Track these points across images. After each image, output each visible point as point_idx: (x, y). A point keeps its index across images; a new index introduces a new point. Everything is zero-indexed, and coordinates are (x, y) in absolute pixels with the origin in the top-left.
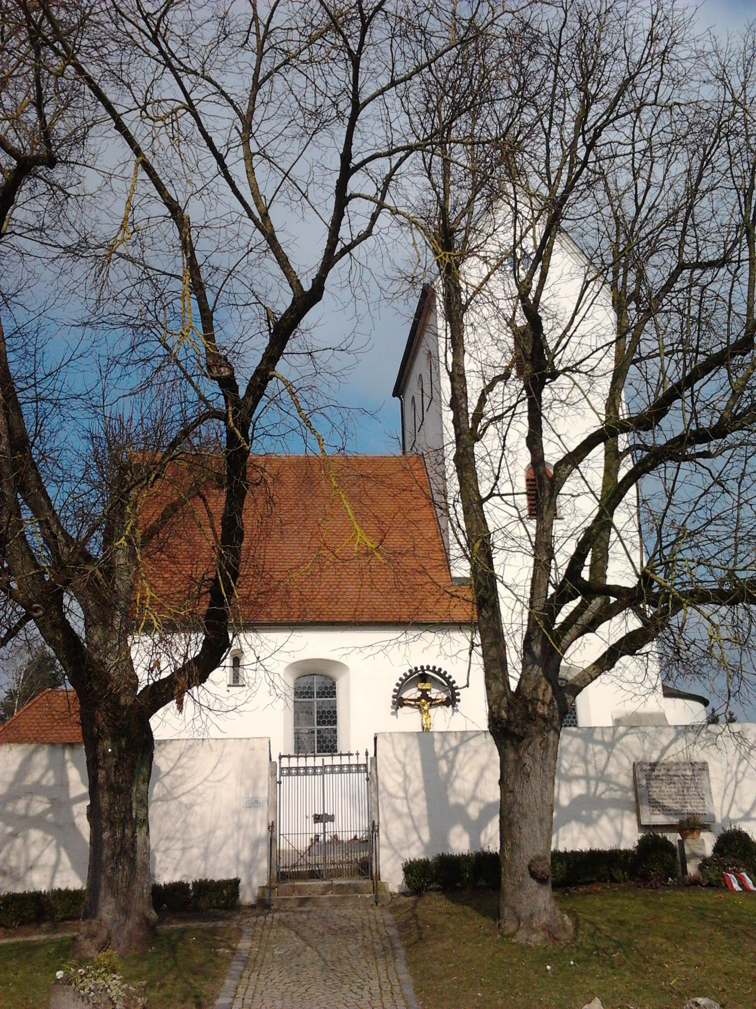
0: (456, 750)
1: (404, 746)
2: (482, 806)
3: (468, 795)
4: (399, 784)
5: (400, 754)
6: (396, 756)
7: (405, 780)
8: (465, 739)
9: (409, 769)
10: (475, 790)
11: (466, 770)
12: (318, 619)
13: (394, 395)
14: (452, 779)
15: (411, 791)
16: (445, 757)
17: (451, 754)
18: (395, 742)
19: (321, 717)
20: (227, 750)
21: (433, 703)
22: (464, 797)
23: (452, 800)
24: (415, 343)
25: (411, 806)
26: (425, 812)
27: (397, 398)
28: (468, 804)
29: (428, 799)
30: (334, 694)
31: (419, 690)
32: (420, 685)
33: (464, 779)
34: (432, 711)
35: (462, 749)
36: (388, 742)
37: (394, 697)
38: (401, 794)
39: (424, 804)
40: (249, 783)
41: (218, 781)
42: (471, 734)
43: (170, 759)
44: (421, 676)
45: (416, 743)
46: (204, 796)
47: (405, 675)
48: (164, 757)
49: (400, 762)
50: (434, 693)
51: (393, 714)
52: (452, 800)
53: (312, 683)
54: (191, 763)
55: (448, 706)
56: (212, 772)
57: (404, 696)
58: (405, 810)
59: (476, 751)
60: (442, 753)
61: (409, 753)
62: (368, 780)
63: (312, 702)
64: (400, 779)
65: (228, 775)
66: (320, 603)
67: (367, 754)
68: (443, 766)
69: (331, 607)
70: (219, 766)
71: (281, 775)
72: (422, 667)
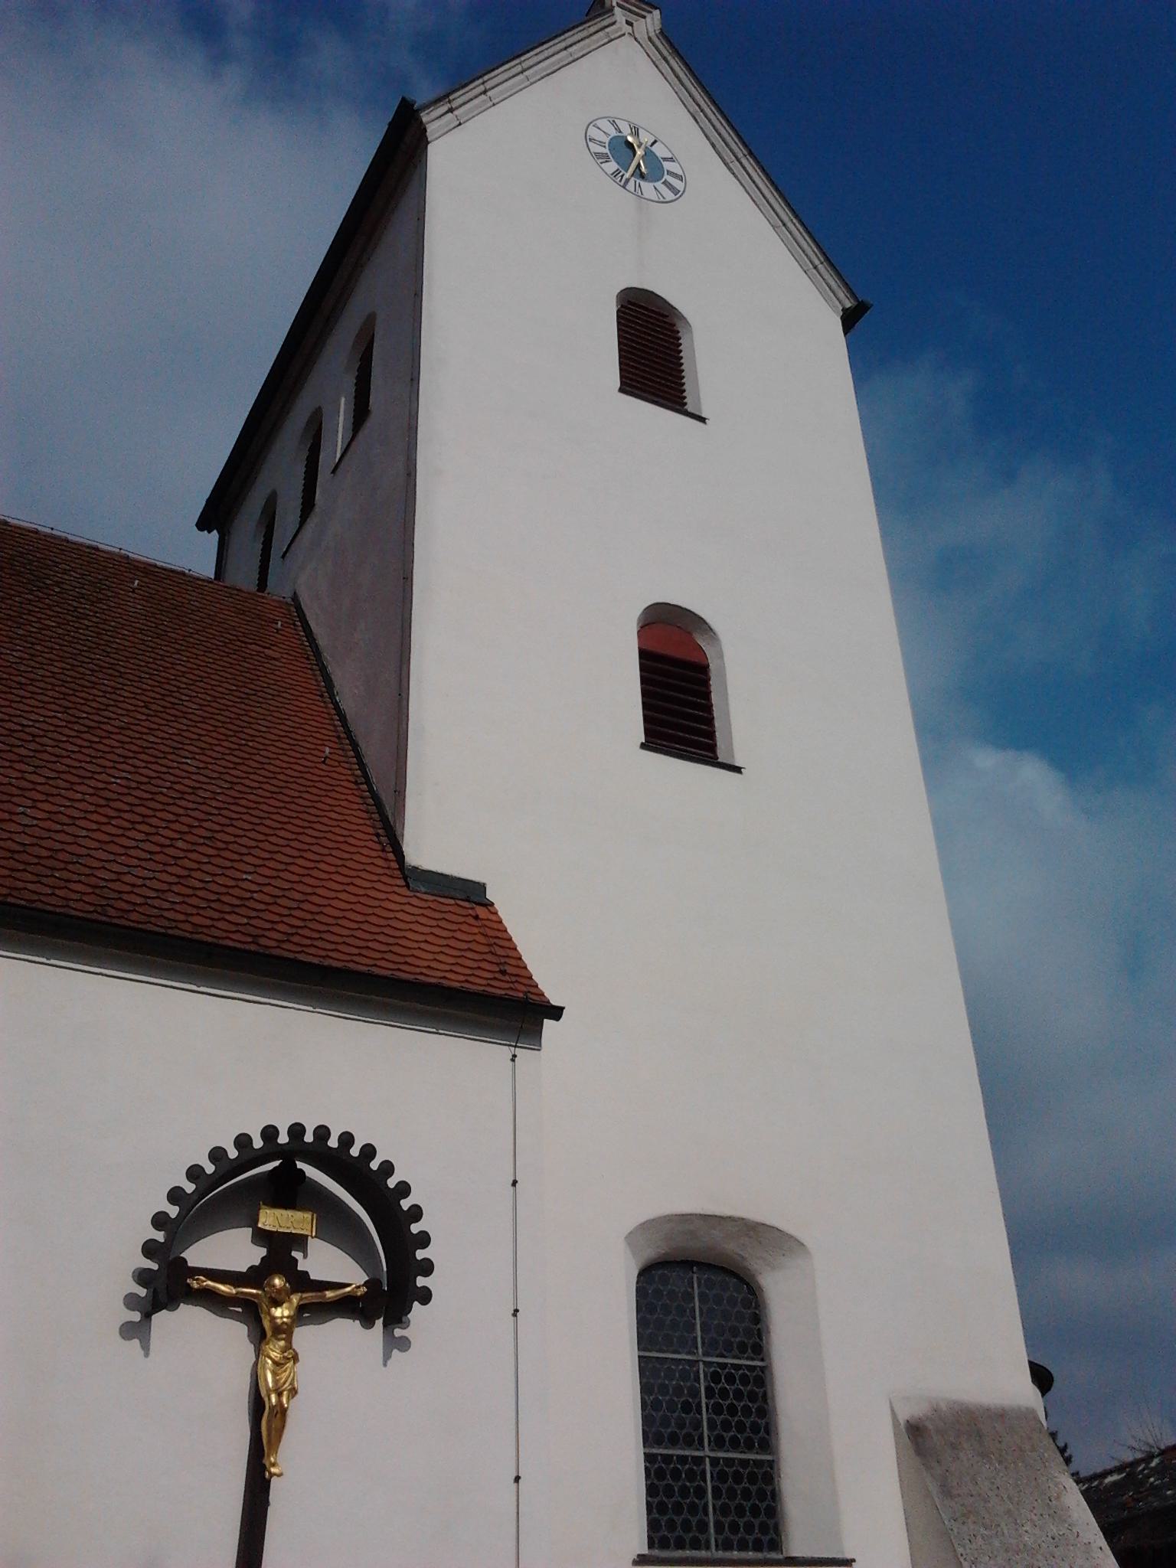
13: (204, 524)
21: (323, 1304)
31: (262, 1237)
32: (271, 1219)
34: (305, 1337)
44: (275, 1173)
47: (217, 1155)
50: (327, 1262)
51: (129, 1331)
55: (368, 1322)
57: (198, 1255)
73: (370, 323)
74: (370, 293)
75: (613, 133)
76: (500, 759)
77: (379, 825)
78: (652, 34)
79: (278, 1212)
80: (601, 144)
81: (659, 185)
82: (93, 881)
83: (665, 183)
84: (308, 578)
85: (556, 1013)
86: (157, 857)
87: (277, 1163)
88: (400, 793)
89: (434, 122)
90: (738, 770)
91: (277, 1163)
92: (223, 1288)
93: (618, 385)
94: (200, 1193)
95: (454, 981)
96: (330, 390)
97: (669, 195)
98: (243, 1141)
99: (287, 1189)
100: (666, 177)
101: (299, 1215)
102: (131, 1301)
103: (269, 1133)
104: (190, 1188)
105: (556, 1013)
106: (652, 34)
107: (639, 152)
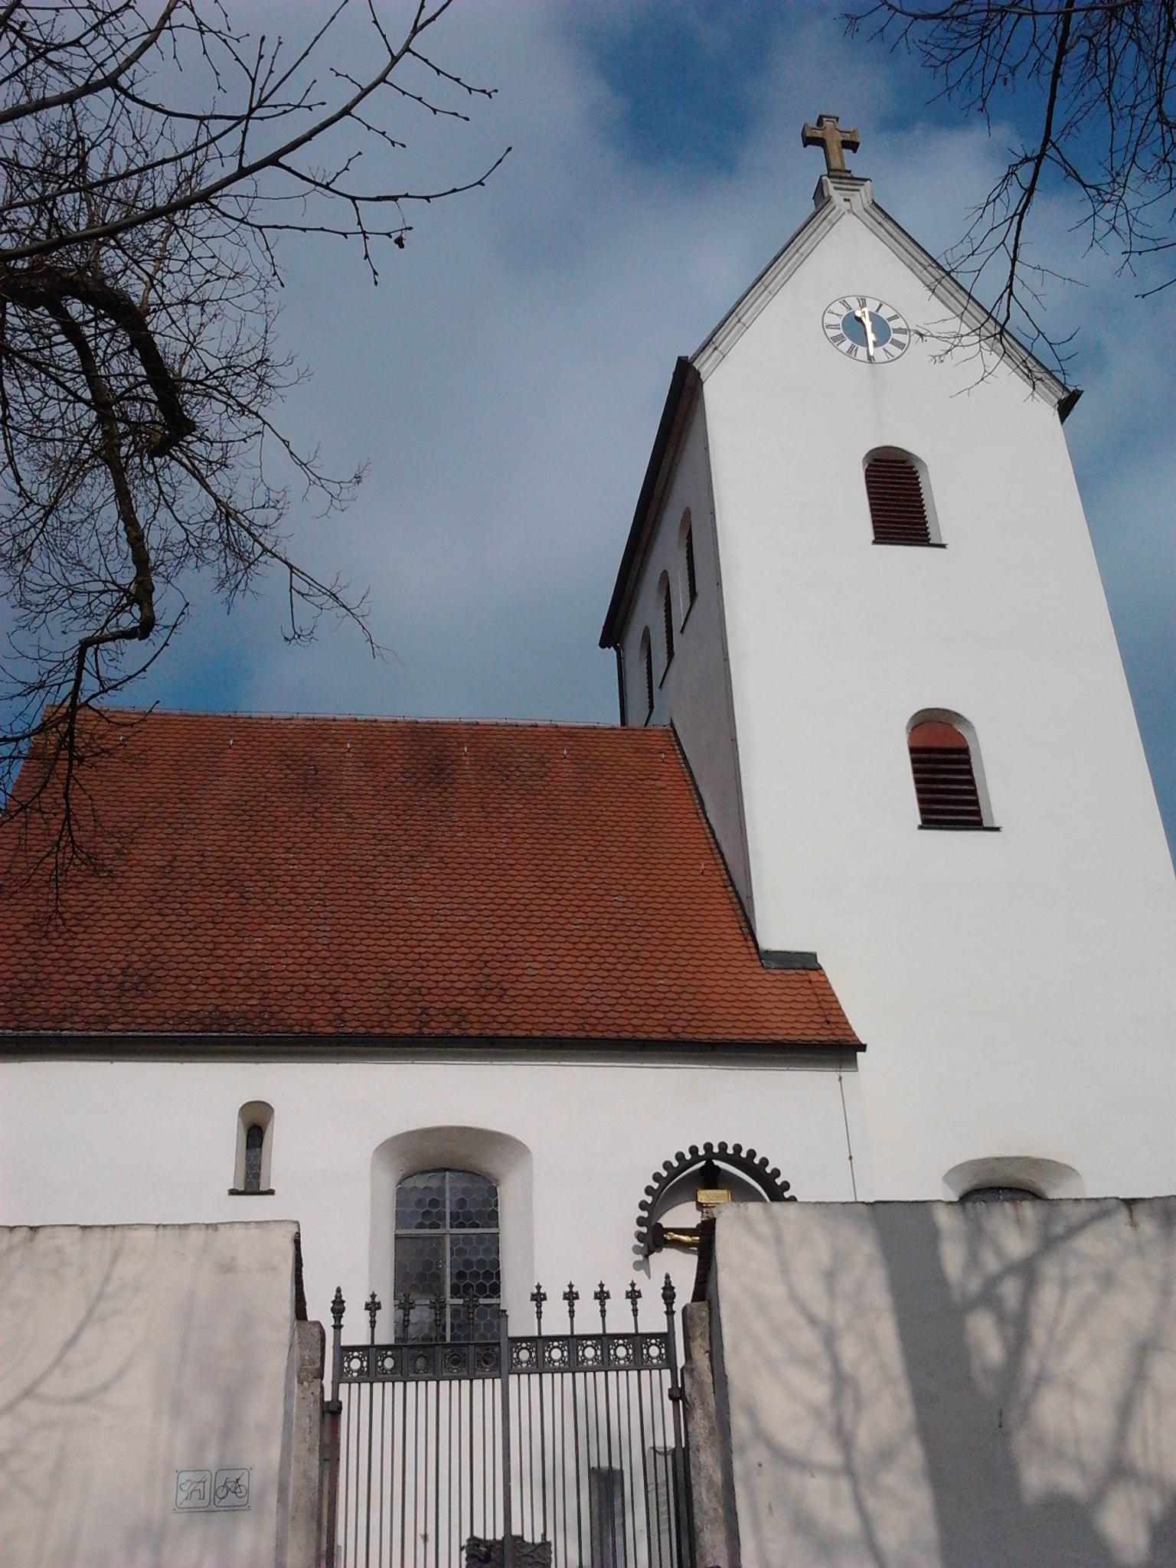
0: (1028, 1271)
2: (1156, 1505)
3: (1095, 1457)
4: (817, 1413)
5: (810, 1287)
6: (794, 1298)
7: (837, 1396)
8: (1059, 1229)
9: (849, 1350)
10: (1121, 1436)
11: (1076, 1355)
12: (456, 1032)
13: (604, 643)
14: (1026, 1389)
15: (864, 1439)
16: (988, 1297)
17: (1010, 1290)
19: (461, 1275)
20: (126, 1269)
22: (1081, 1467)
23: (1036, 1477)
24: (657, 492)
25: (871, 1503)
26: (930, 1531)
27: (611, 652)
28: (1099, 1497)
29: (938, 1476)
30: (493, 1218)
31: (700, 1206)
32: (704, 1196)
33: (1070, 1387)
35: (1050, 1269)
37: (641, 1222)
38: (827, 1453)
39: (922, 1499)
40: (205, 1407)
41: (81, 1399)
42: (1077, 1213)
46: (15, 1464)
47: (667, 1165)
49: (813, 1321)
51: (638, 1266)
52: (1036, 1477)
53: (441, 1191)
56: (59, 1360)
57: (668, 1220)
58: (847, 1522)
59: (1107, 1280)
60: (974, 1285)
61: (846, 1283)
62: (677, 1395)
63: (440, 1238)
64: (820, 1392)
65: (121, 1373)
66: (460, 999)
67: (669, 1294)
68: (986, 1337)
69: (486, 1006)
70: (89, 1337)
71: (341, 1376)
73: (687, 514)
75: (845, 312)
76: (818, 853)
77: (742, 919)
78: (867, 206)
79: (708, 1192)
80: (836, 327)
81: (888, 346)
83: (894, 342)
84: (676, 707)
86: (607, 980)
87: (703, 1163)
88: (750, 897)
89: (703, 366)
90: (997, 829)
91: (703, 1163)
92: (685, 1238)
93: (872, 538)
94: (670, 1178)
95: (795, 1036)
96: (667, 554)
97: (896, 351)
98: (680, 1156)
99: (711, 1178)
100: (894, 336)
101: (719, 1192)
103: (693, 1150)
104: (656, 1186)
105: (863, 1048)
106: (867, 206)
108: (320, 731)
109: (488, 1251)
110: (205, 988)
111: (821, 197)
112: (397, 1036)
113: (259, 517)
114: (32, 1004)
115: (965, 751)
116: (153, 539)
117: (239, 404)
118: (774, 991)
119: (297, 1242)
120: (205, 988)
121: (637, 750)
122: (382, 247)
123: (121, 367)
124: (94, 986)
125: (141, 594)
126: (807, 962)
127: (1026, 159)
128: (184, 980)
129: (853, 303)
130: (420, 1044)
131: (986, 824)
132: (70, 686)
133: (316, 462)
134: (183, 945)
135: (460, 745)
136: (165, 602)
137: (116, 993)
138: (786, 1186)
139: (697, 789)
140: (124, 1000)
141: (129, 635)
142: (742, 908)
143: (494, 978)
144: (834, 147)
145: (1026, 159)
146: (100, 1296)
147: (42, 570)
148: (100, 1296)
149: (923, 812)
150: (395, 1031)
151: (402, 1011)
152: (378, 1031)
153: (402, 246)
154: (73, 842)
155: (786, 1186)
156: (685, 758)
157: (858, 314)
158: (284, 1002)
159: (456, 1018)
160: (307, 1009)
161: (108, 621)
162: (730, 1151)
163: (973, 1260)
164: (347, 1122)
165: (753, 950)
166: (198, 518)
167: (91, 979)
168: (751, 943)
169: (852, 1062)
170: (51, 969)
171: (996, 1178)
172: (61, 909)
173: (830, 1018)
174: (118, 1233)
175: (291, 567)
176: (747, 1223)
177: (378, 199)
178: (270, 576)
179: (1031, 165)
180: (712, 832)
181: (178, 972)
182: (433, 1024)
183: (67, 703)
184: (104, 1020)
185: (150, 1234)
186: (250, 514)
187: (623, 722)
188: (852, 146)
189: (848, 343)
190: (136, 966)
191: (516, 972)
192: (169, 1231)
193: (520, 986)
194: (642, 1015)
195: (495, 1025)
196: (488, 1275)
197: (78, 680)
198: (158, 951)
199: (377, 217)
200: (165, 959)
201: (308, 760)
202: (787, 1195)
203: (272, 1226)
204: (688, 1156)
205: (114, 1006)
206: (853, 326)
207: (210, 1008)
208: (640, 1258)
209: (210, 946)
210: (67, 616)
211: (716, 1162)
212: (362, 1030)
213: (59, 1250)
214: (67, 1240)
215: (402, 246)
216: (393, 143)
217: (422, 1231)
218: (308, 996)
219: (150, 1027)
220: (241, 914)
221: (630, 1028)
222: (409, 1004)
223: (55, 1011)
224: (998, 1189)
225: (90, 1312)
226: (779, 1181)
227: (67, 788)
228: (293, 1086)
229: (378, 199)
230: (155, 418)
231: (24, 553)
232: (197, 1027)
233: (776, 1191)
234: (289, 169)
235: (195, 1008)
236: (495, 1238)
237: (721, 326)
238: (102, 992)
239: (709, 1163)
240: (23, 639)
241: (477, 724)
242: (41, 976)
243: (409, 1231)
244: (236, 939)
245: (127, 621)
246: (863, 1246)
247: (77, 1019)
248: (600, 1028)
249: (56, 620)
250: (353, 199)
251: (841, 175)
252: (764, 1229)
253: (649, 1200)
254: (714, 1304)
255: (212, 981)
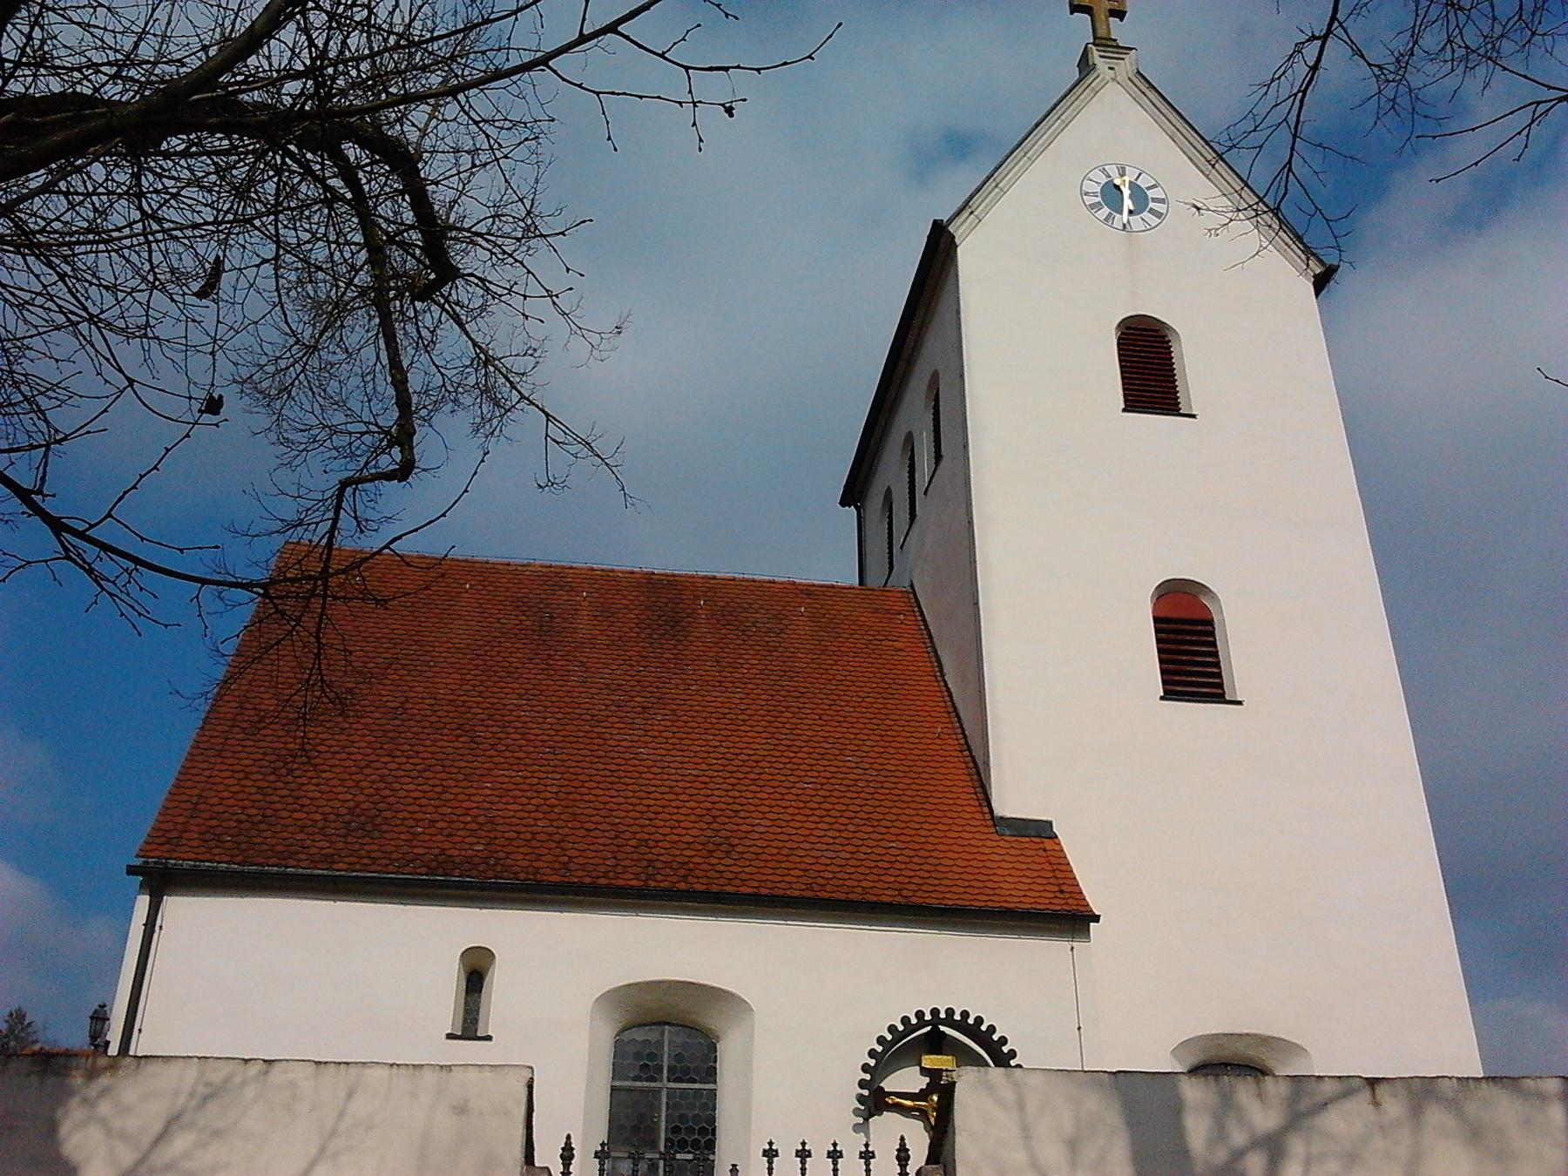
1: (1068, 1126)
12: (682, 886)
13: (844, 502)
18: (1032, 1105)
19: (676, 1130)
20: (361, 1106)
30: (711, 1074)
31: (924, 1072)
32: (929, 1061)
35: (1297, 1146)
36: (1001, 1103)
42: (1328, 1088)
43: (124, 1136)
45: (1112, 1116)
48: (104, 1123)
53: (660, 1044)
54: (209, 1156)
57: (889, 1084)
61: (1089, 1153)
67: (903, 1156)
72: (935, 1012)
73: (935, 377)
74: (930, 356)
75: (1104, 180)
76: (1058, 716)
77: (977, 784)
81: (1146, 215)
82: (803, 866)
83: (1152, 211)
84: (919, 570)
85: (1096, 919)
88: (987, 763)
89: (957, 230)
92: (908, 1103)
94: (885, 1052)
96: (913, 415)
97: (1154, 220)
99: (936, 1043)
100: (1151, 205)
102: (856, 1112)
104: (880, 1049)
105: (1096, 919)
107: (1126, 192)
108: (557, 579)
109: (705, 1106)
110: (433, 831)
111: (1085, 66)
112: (622, 888)
113: (519, 364)
114: (259, 840)
115: (1210, 623)
116: (415, 382)
117: (504, 252)
118: (1007, 858)
119: (530, 1087)
120: (433, 831)
121: (876, 611)
122: (712, 116)
123: (396, 211)
124: (320, 825)
125: (403, 436)
126: (1041, 831)
127: (1313, 38)
128: (411, 822)
129: (1113, 171)
130: (627, 896)
131: (1222, 695)
132: (325, 527)
133: (579, 312)
134: (412, 787)
135: (697, 598)
136: (425, 444)
137: (343, 832)
138: (1013, 1054)
139: (935, 651)
140: (350, 839)
141: (388, 476)
142: (978, 774)
143: (723, 833)
144: (1101, 16)
145: (1313, 38)
146: (333, 1133)
147: (302, 410)
148: (333, 1133)
149: (1164, 682)
150: (621, 882)
151: (627, 863)
152: (603, 881)
153: (731, 115)
154: (322, 681)
155: (1013, 1054)
156: (924, 620)
157: (1117, 182)
158: (510, 849)
159: (682, 872)
160: (533, 857)
161: (367, 463)
162: (957, 1017)
163: (1220, 1133)
164: (569, 968)
165: (988, 816)
166: (457, 363)
167: (318, 817)
168: (986, 810)
169: (1085, 933)
170: (278, 806)
171: (1226, 1054)
172: (308, 747)
173: (1064, 888)
174: (353, 1070)
175: (547, 415)
176: (989, 1087)
177: (711, 69)
178: (526, 422)
179: (1318, 43)
180: (951, 696)
181: (406, 815)
182: (659, 877)
183: (325, 541)
184: (329, 860)
185: (385, 1072)
186: (508, 362)
187: (861, 582)
188: (1120, 14)
189: (1106, 210)
190: (364, 806)
191: (744, 828)
192: (402, 1070)
193: (748, 842)
194: (871, 877)
195: (722, 881)
196: (703, 1131)
197: (335, 520)
198: (387, 792)
199: (713, 88)
200: (392, 800)
201: (539, 605)
202: (1013, 1063)
203: (506, 1070)
204: (914, 1021)
205: (341, 845)
206: (1112, 193)
207: (436, 851)
208: (861, 1120)
209: (439, 789)
210: (328, 455)
211: (942, 1028)
212: (588, 880)
213: (293, 1084)
214: (301, 1074)
215: (731, 115)
216: (727, 15)
217: (639, 1084)
218: (534, 843)
219: (374, 867)
220: (470, 758)
221: (859, 890)
222: (635, 856)
223: (280, 848)
224: (1226, 1065)
225: (322, 1149)
226: (1005, 1049)
227: (319, 628)
228: (521, 936)
229: (711, 69)
230: (419, 264)
231: (285, 390)
232: (424, 870)
233: (1001, 1057)
234: (627, 38)
235: (421, 851)
236: (713, 1093)
237: (978, 190)
238: (329, 831)
239: (935, 1029)
240: (285, 478)
241: (714, 578)
242: (269, 812)
243: (628, 1083)
244: (464, 784)
245: (386, 463)
246: (1107, 1113)
247: (302, 857)
248: (828, 888)
249: (315, 460)
250: (687, 68)
251: (1104, 42)
252: (1008, 1095)
253: (872, 1062)
254: (949, 1167)
255: (439, 825)
